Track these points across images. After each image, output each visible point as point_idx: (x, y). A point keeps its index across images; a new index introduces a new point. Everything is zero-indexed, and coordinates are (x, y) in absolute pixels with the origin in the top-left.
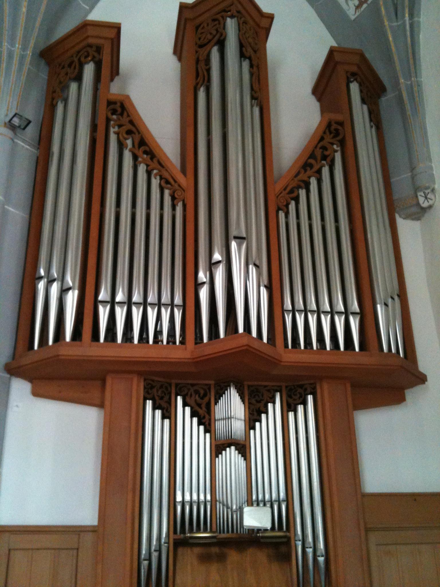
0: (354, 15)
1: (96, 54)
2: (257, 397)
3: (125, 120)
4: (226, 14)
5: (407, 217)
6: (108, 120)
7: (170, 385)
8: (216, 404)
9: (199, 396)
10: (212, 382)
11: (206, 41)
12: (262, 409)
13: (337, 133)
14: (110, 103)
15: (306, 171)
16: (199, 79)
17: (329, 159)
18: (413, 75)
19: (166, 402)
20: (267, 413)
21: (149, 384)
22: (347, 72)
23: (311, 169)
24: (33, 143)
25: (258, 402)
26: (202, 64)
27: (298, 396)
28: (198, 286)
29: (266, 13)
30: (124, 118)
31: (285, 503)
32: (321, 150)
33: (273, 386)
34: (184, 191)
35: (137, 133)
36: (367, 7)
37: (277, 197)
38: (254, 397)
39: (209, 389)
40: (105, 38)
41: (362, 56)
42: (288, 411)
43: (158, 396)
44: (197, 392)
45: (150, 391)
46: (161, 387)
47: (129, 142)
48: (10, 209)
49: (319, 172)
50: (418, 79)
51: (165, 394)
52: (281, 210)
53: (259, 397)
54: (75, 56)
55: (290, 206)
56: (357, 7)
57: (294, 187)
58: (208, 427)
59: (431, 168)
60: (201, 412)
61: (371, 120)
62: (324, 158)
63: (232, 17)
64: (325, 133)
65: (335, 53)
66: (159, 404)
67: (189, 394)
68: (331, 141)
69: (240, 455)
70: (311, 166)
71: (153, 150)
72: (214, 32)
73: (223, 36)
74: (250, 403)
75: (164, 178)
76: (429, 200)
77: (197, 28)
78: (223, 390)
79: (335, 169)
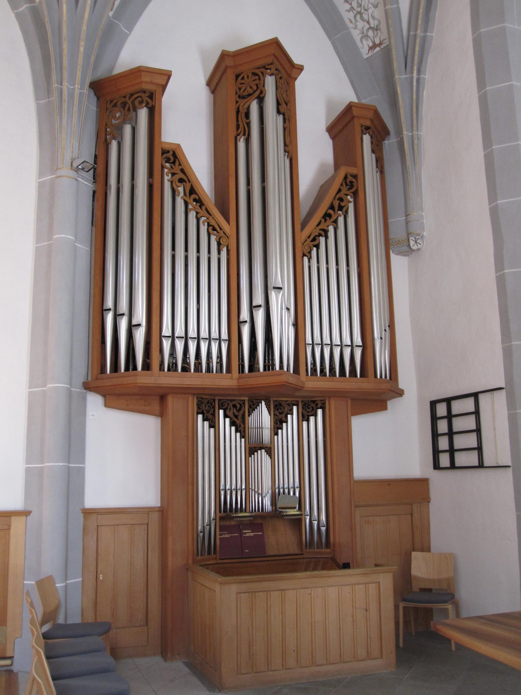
0: (368, 54)
1: (149, 100)
2: (279, 409)
3: (177, 169)
4: (266, 71)
5: (399, 253)
6: (163, 167)
7: (214, 400)
8: (249, 416)
9: (236, 409)
10: (246, 399)
11: (246, 93)
12: (284, 419)
13: (351, 185)
14: (164, 152)
15: (326, 220)
16: (240, 130)
17: (344, 209)
18: (415, 128)
19: (212, 414)
20: (287, 422)
21: (200, 401)
22: (362, 126)
23: (330, 219)
24: (90, 178)
25: (281, 413)
26: (242, 115)
27: (311, 409)
28: (240, 323)
29: (297, 65)
30: (176, 167)
31: (299, 489)
32: (339, 201)
33: (292, 401)
34: (228, 237)
35: (188, 182)
36: (379, 51)
37: (303, 244)
38: (277, 410)
39: (244, 403)
40: (157, 84)
41: (376, 112)
42: (303, 421)
43: (206, 410)
44: (234, 406)
45: (200, 407)
46: (208, 403)
47: (181, 189)
48: (78, 245)
49: (336, 222)
50: (419, 133)
51: (211, 409)
52: (306, 256)
53: (281, 409)
54: (127, 97)
55: (312, 252)
56: (371, 48)
57: (316, 236)
58: (243, 434)
59: (422, 217)
60: (238, 422)
61: (377, 167)
62: (341, 208)
63: (271, 75)
64: (342, 185)
65: (353, 108)
66: (207, 416)
67: (229, 407)
68: (347, 193)
69: (267, 455)
70: (330, 216)
71: (202, 198)
72: (255, 88)
73: (264, 93)
74: (274, 415)
75: (212, 226)
76: (418, 244)
77: (237, 76)
78: (256, 405)
79: (348, 217)
